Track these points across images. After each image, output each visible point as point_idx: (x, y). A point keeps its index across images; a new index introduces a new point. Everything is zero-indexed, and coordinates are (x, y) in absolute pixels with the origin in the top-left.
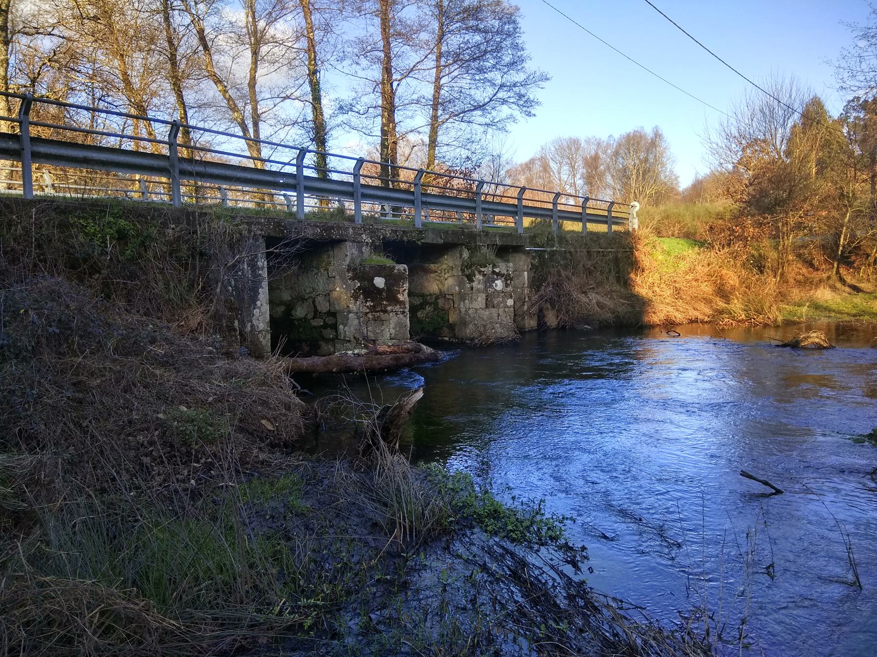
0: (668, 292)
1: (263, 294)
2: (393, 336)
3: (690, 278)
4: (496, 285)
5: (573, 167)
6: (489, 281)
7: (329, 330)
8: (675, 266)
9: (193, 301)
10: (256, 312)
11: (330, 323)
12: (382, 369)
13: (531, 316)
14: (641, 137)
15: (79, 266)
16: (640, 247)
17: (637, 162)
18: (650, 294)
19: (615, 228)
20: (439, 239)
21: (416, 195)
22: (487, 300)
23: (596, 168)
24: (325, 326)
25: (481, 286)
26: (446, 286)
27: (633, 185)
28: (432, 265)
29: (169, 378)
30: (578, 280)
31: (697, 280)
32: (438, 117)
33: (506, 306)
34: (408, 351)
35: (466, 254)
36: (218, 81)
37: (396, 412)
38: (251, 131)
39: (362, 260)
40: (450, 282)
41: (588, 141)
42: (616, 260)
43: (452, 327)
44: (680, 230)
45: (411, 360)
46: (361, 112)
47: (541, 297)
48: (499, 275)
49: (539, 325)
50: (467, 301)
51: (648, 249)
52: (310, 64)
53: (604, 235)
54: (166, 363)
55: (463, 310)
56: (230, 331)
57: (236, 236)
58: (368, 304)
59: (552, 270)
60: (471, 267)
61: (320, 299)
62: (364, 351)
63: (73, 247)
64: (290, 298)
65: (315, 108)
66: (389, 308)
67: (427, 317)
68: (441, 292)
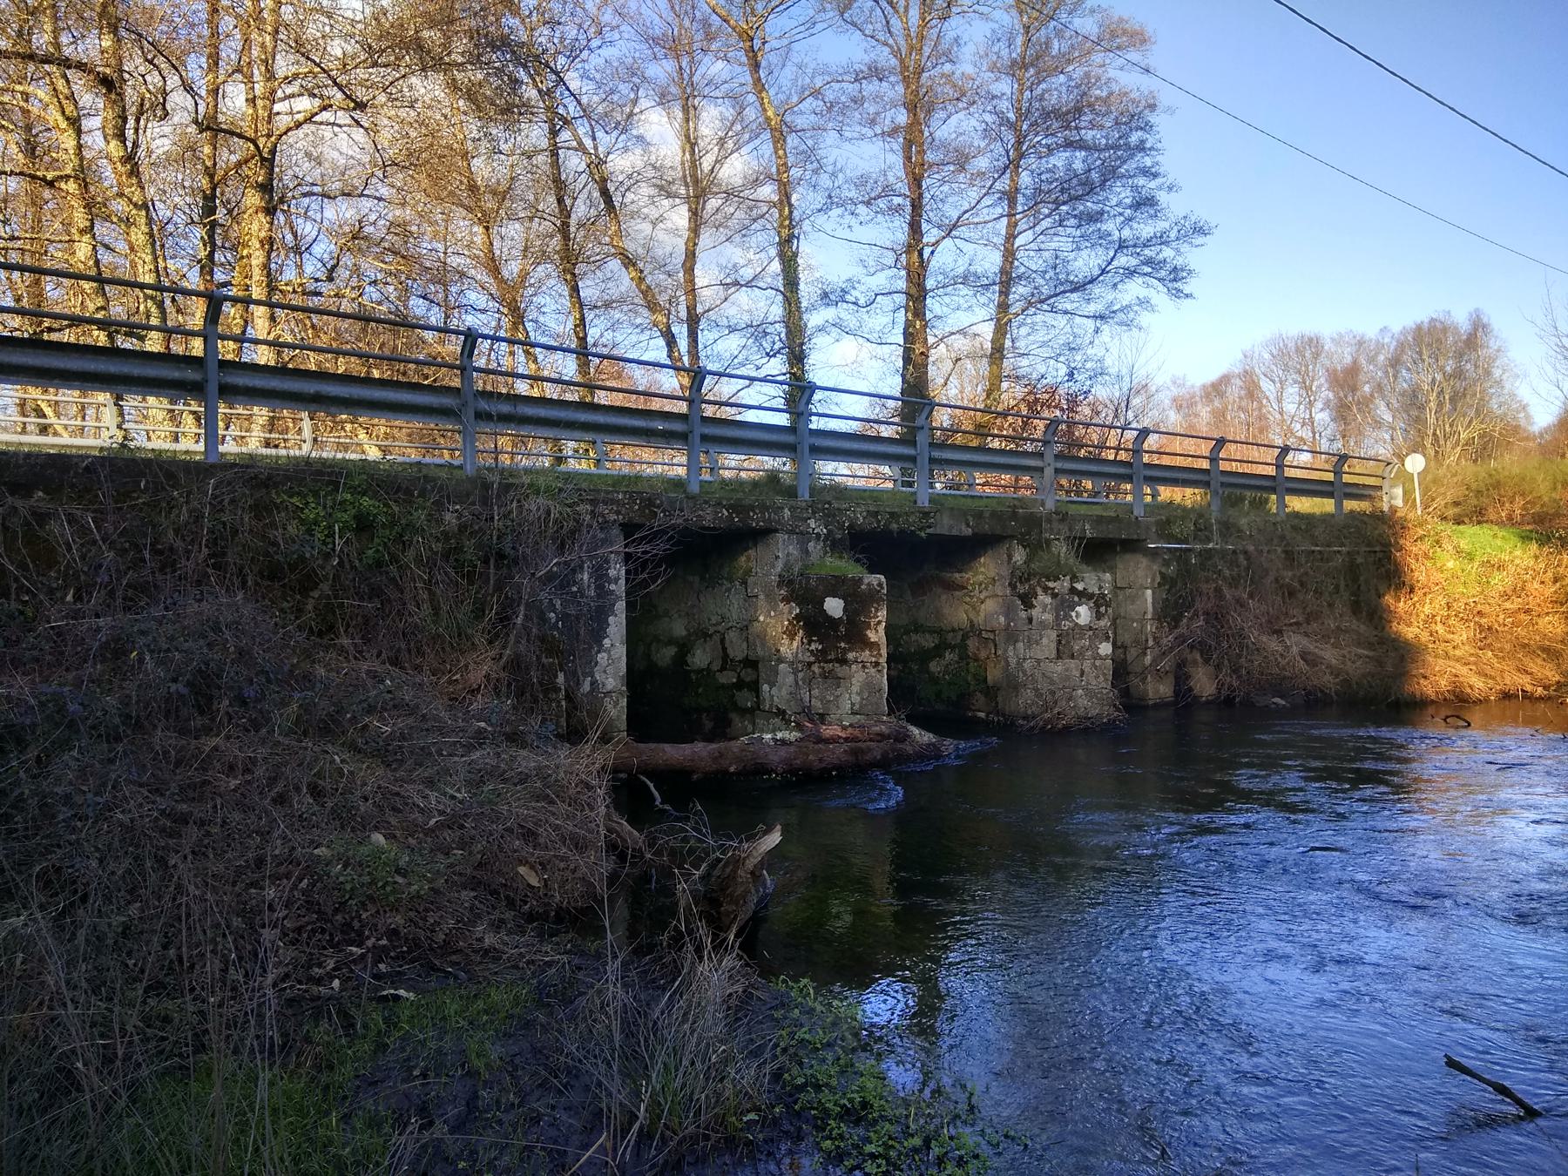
0: (1463, 634)
1: (617, 625)
2: (857, 707)
3: (1514, 606)
4: (1078, 615)
5: (1308, 389)
6: (1064, 605)
7: (745, 693)
8: (1484, 582)
9: (481, 640)
10: (602, 657)
11: (748, 679)
12: (827, 771)
13: (1160, 676)
14: (1445, 330)
15: (283, 577)
16: (1406, 543)
17: (1439, 377)
18: (1425, 637)
19: (1350, 505)
20: (964, 527)
21: (965, 450)
22: (1059, 642)
23: (1354, 389)
24: (740, 684)
25: (1048, 617)
26: (982, 615)
27: (1431, 420)
28: (957, 575)
29: (371, 776)
30: (1264, 608)
31: (1527, 611)
32: (1008, 306)
33: (1097, 656)
34: (882, 737)
35: (1019, 556)
36: (629, 262)
37: (728, 870)
38: (683, 344)
39: (806, 567)
40: (990, 606)
41: (1338, 340)
42: (1352, 570)
43: (991, 692)
44: (1524, 508)
45: (885, 755)
46: (862, 302)
47: (1181, 640)
48: (1084, 595)
49: (1177, 693)
50: (1020, 645)
51: (1425, 546)
52: (781, 226)
53: (1326, 519)
54: (385, 753)
55: (1013, 661)
56: (546, 692)
57: (569, 525)
58: (813, 647)
59: (1204, 587)
60: (1028, 580)
61: (732, 636)
62: (793, 736)
63: (275, 544)
64: (684, 633)
65: (787, 300)
66: (851, 656)
67: (946, 672)
68: (972, 626)
